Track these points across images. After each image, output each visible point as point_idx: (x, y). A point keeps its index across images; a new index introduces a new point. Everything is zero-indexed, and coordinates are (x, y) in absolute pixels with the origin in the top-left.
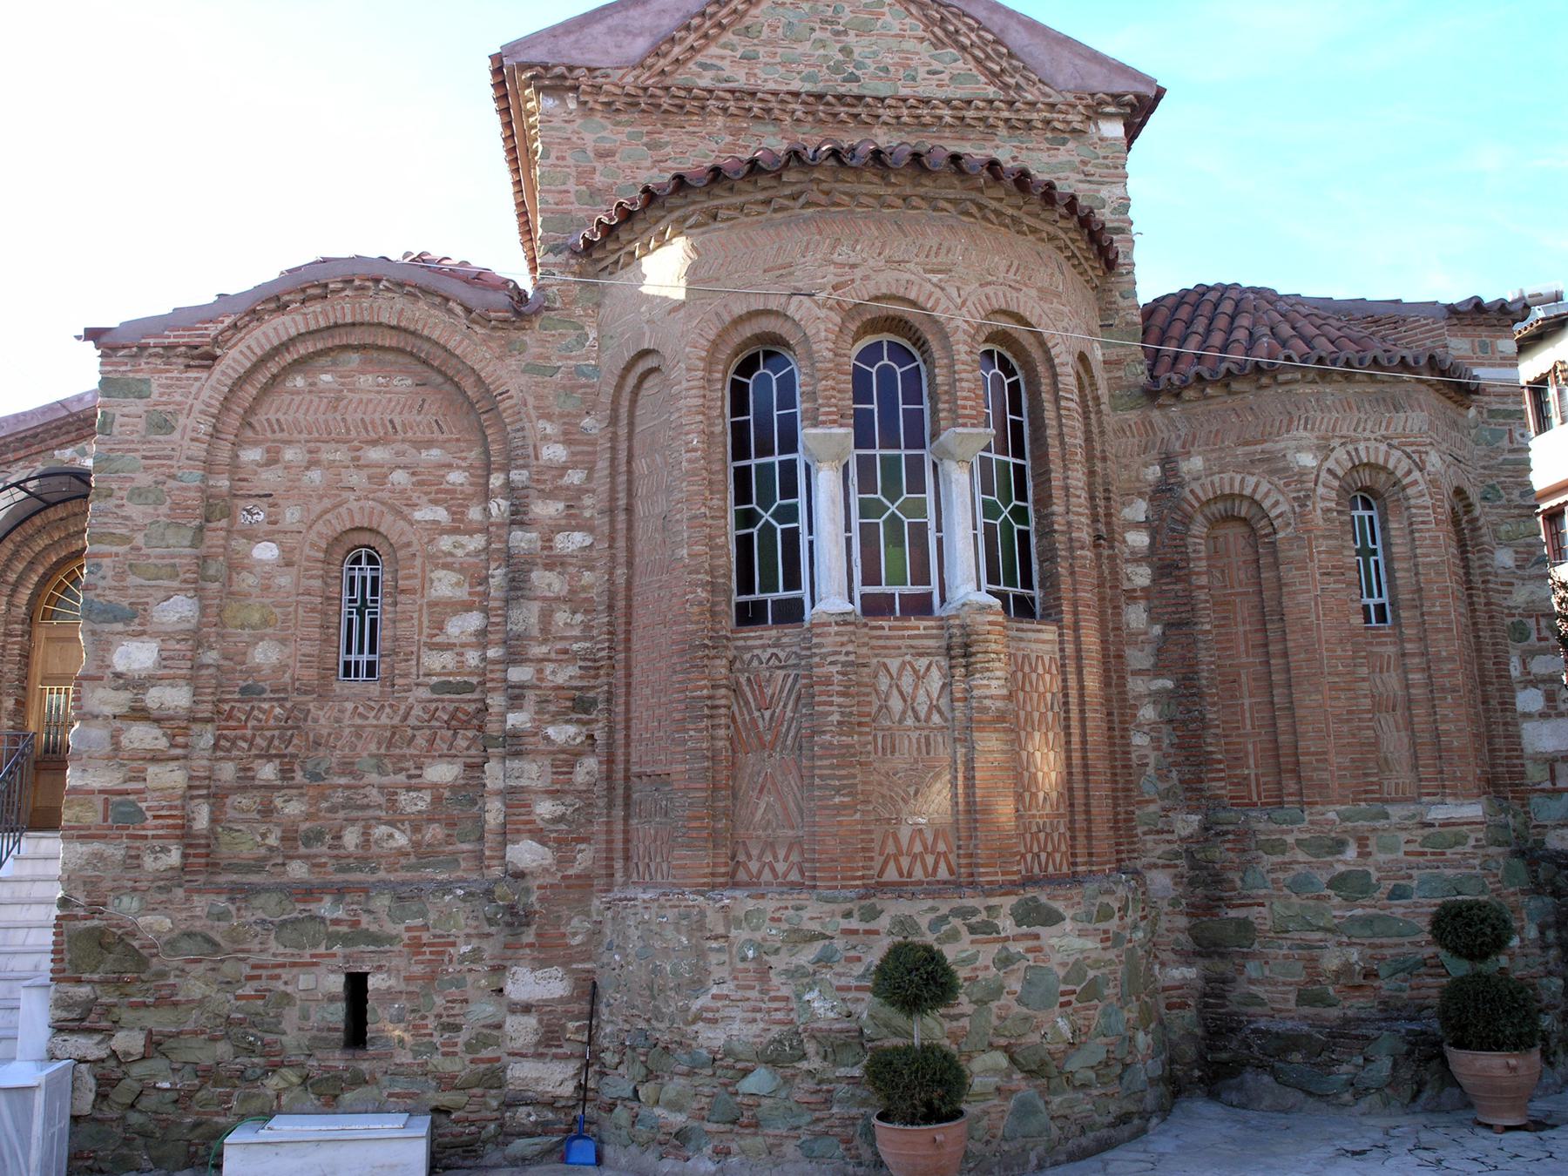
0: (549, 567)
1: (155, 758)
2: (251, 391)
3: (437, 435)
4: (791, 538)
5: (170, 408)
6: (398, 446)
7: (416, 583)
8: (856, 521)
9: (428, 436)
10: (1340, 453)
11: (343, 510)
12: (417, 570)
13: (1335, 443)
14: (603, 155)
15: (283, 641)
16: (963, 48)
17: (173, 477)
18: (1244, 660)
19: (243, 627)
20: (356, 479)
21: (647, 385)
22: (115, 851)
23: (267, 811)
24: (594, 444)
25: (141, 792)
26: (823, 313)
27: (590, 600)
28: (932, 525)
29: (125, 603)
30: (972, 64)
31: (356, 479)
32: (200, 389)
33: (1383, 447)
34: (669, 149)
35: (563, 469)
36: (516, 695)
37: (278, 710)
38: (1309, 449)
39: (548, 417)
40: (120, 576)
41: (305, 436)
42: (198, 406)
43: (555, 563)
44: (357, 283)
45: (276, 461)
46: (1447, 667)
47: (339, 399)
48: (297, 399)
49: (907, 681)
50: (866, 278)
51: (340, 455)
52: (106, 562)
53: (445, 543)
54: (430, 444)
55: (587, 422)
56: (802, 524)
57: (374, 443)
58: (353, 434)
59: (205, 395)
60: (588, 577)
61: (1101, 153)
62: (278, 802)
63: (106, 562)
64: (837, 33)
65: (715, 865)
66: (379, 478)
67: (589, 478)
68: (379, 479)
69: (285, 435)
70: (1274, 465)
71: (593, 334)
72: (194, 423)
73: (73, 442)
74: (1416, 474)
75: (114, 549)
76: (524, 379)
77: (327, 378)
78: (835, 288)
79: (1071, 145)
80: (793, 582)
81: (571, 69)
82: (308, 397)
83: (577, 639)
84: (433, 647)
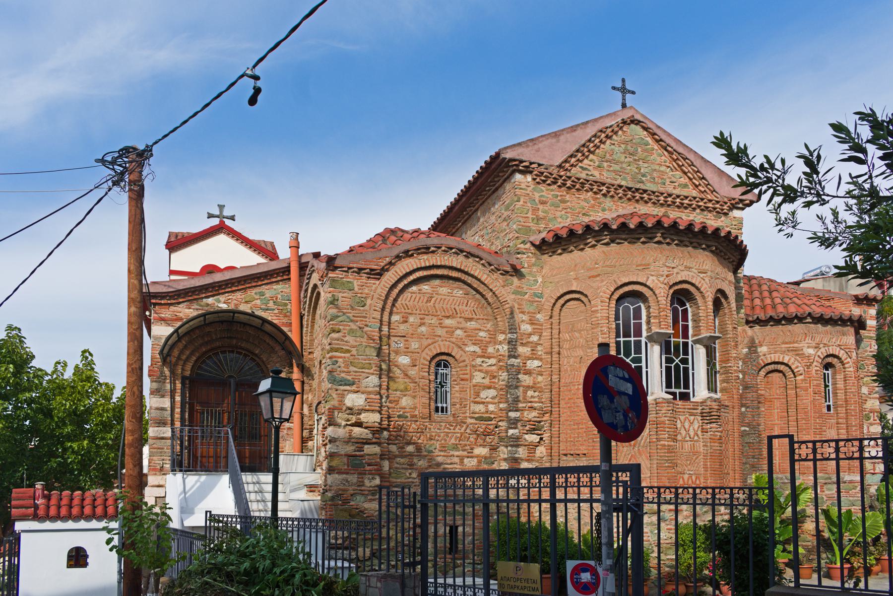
0: (525, 374)
1: (368, 442)
2: (396, 291)
3: (474, 316)
4: (686, 370)
5: (364, 296)
6: (459, 319)
7: (467, 376)
8: (664, 365)
9: (470, 316)
10: (823, 350)
11: (436, 345)
12: (468, 372)
13: (821, 346)
14: (543, 203)
15: (414, 397)
16: (685, 173)
17: (367, 326)
18: (777, 422)
19: (396, 390)
20: (440, 331)
21: (568, 304)
22: (353, 478)
23: (411, 465)
24: (542, 325)
25: (362, 456)
26: (662, 286)
27: (541, 387)
28: (691, 368)
29: (349, 378)
30: (687, 180)
31: (440, 331)
32: (376, 288)
33: (838, 349)
34: (569, 204)
35: (530, 335)
36: (513, 423)
37: (413, 425)
38: (812, 347)
39: (523, 313)
40: (347, 366)
41: (418, 312)
42: (376, 296)
43: (528, 373)
44: (443, 248)
45: (406, 322)
46: (854, 428)
47: (432, 297)
48: (414, 295)
49: (687, 425)
50: (677, 273)
51: (434, 321)
52: (340, 360)
53: (479, 361)
54: (471, 319)
55: (539, 316)
56: (643, 364)
57: (448, 317)
58: (439, 313)
59: (379, 290)
60: (540, 378)
61: (734, 223)
62: (415, 461)
63: (340, 360)
64: (635, 160)
65: (540, 501)
66: (451, 331)
67: (540, 339)
68: (451, 331)
69: (410, 311)
70: (798, 352)
71: (540, 280)
72: (374, 304)
73: (213, 296)
74: (849, 359)
75: (343, 355)
76: (513, 296)
77: (426, 287)
78: (667, 276)
79: (723, 218)
80: (686, 386)
81: (531, 163)
82: (418, 295)
83: (536, 402)
84: (476, 403)
